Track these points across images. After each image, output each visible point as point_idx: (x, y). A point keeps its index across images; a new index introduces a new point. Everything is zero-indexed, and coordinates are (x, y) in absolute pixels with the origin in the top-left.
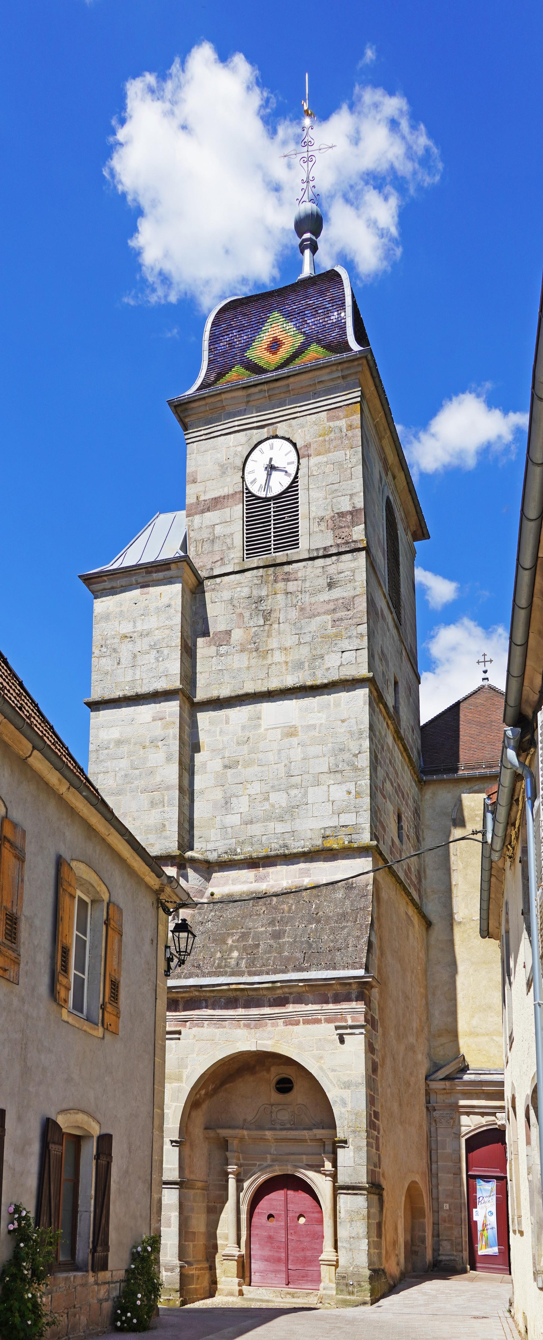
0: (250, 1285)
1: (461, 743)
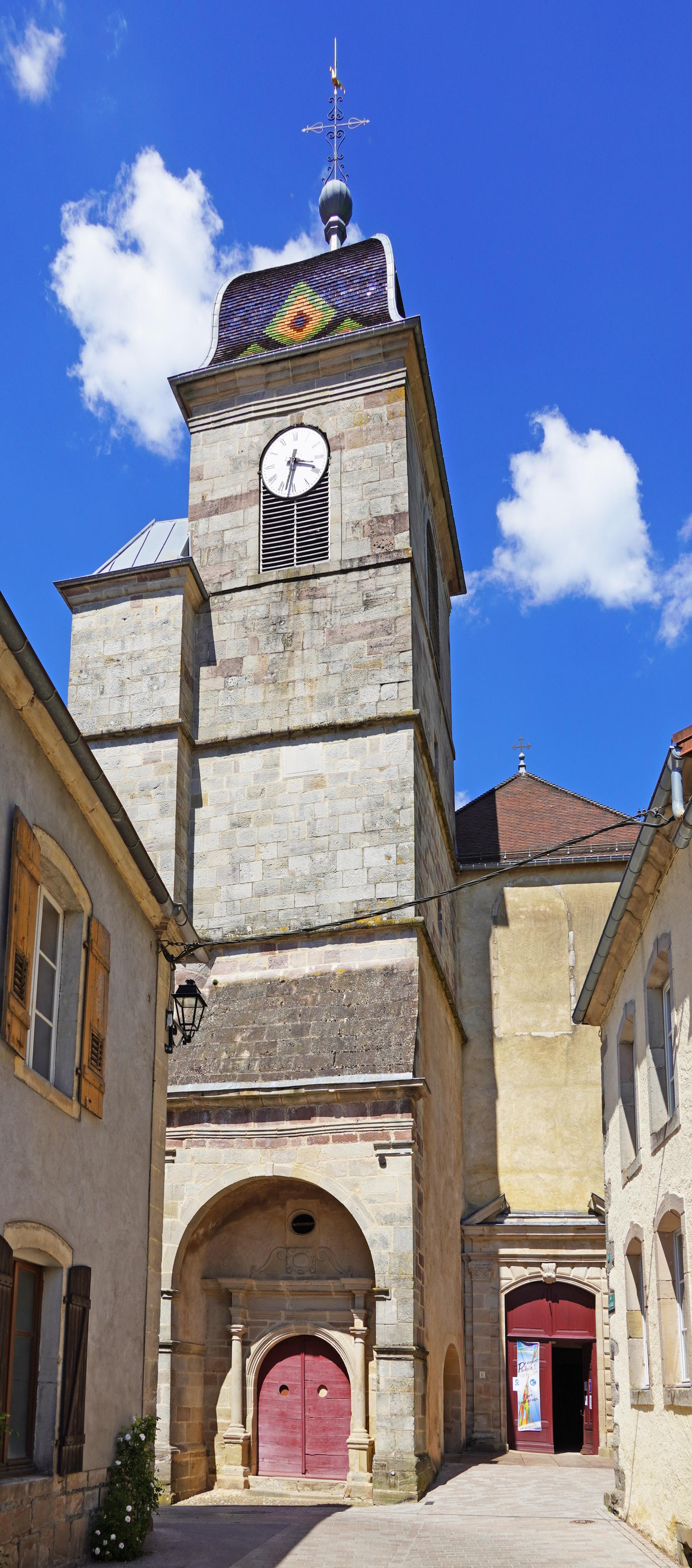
0: (257, 1475)
1: (499, 832)
